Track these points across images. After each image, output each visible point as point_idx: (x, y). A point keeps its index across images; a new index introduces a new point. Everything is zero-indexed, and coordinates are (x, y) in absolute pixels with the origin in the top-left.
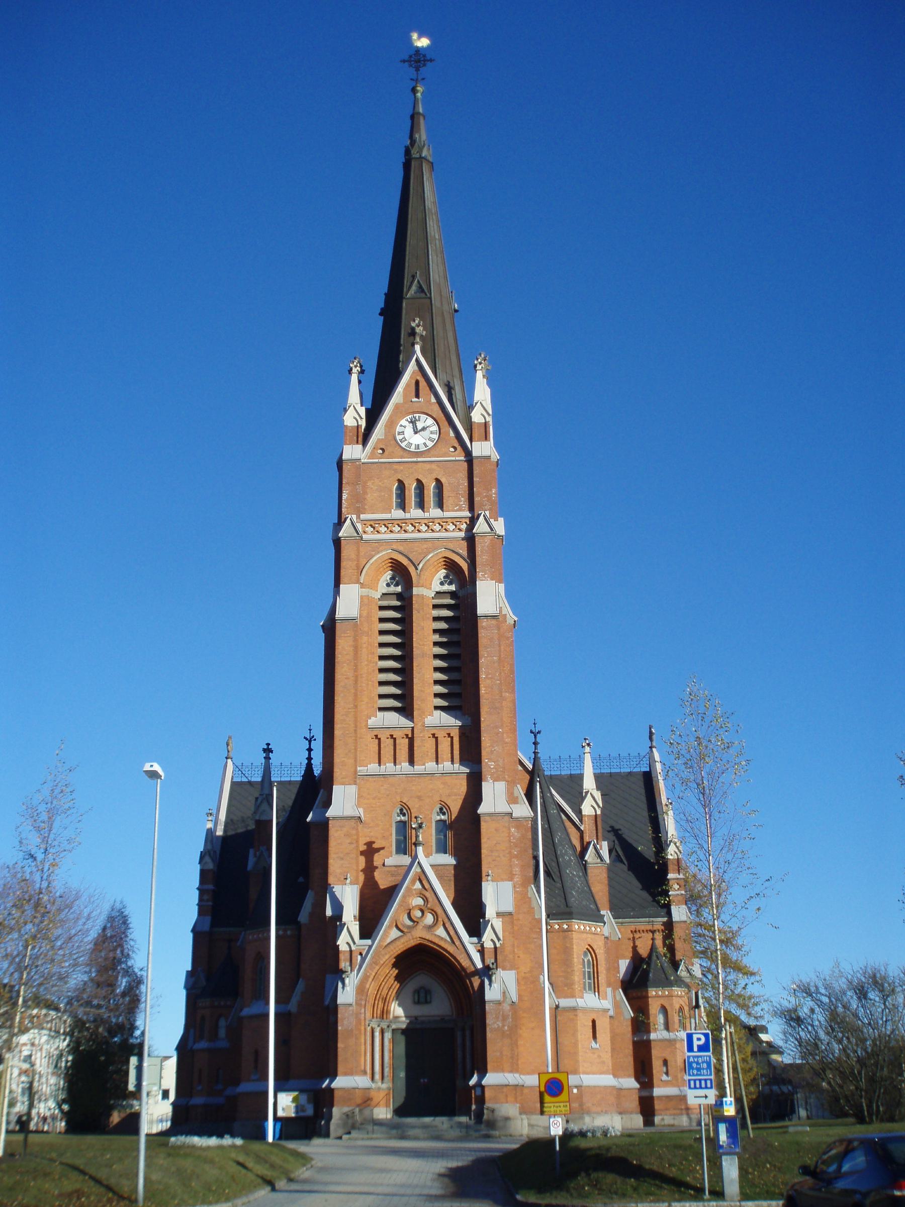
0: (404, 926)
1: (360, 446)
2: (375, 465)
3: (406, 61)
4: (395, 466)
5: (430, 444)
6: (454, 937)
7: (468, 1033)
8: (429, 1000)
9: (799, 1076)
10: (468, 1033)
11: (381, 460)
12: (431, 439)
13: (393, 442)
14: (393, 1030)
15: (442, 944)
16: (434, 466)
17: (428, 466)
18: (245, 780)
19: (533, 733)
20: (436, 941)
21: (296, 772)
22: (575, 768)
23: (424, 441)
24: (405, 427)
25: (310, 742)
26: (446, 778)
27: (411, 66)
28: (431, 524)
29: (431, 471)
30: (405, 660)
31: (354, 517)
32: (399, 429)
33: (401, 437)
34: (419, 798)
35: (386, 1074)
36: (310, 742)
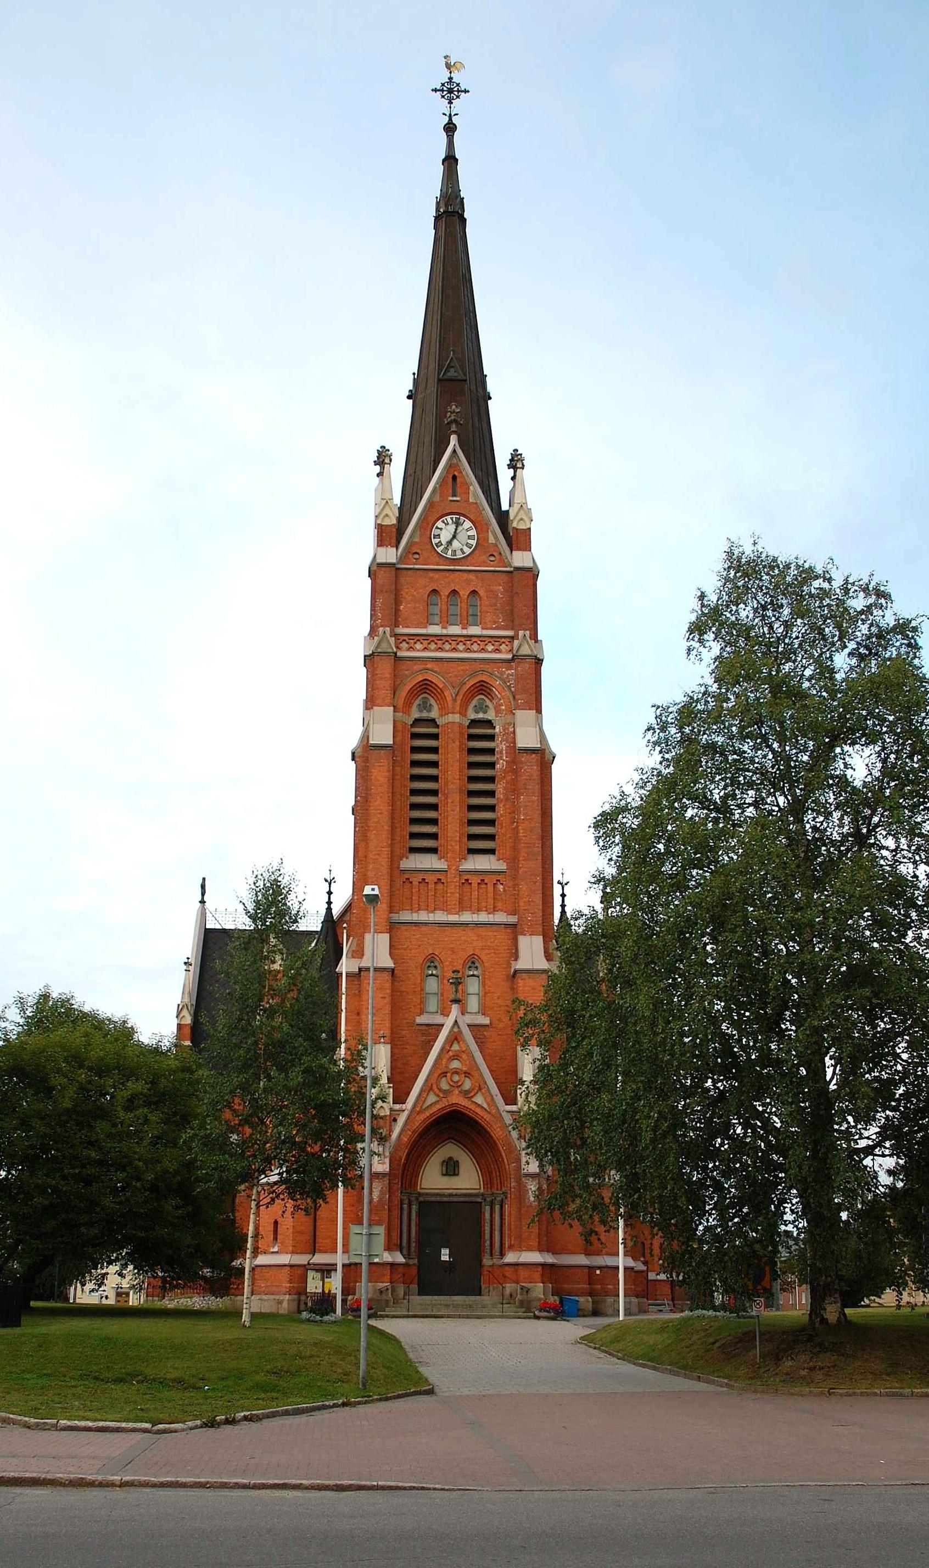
0: (440, 1090)
1: (394, 549)
2: (410, 572)
3: (439, 90)
4: (431, 574)
5: (468, 551)
6: (492, 1102)
7: (497, 1207)
8: (457, 1173)
9: (145, 1143)
10: (497, 1207)
11: (416, 567)
12: (468, 545)
13: (429, 546)
14: (420, 1203)
15: (478, 1110)
16: (472, 576)
17: (465, 576)
18: (218, 927)
19: (561, 884)
20: (472, 1107)
21: (312, 921)
22: (312, 924)
23: (461, 547)
24: (441, 529)
25: (330, 884)
26: (480, 929)
27: (458, 85)
28: (468, 642)
29: (468, 582)
30: (438, 796)
31: (388, 629)
32: (435, 531)
33: (437, 540)
34: (452, 950)
35: (413, 1250)
36: (330, 884)
